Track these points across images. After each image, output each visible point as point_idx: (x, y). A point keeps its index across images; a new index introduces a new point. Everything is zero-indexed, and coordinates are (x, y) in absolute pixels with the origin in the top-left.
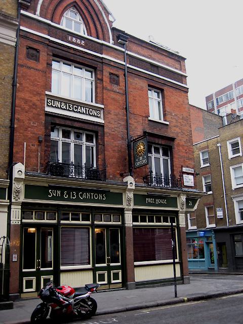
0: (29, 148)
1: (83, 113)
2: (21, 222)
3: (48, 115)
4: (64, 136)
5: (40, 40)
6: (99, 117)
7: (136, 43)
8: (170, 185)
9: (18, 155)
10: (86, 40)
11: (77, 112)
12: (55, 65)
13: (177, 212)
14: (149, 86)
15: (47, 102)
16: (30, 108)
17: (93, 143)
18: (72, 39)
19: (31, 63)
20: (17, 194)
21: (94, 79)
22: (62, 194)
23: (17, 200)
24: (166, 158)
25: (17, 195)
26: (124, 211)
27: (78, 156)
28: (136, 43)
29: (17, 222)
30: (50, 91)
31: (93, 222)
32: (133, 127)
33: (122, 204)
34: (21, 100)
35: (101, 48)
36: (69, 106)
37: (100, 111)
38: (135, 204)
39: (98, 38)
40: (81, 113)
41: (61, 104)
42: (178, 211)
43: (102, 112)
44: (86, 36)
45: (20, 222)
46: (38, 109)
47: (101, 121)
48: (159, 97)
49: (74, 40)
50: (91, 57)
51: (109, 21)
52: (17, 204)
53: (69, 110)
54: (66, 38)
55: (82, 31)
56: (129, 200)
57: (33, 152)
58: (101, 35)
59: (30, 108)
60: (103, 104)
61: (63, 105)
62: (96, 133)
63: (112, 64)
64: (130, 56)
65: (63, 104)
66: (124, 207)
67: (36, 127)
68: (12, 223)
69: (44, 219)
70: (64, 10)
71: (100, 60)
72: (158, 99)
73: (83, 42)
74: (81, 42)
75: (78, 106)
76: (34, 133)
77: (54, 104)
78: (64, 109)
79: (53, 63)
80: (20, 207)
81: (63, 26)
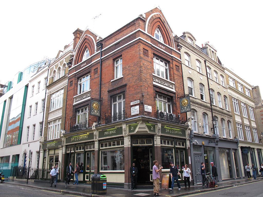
3: (155, 86)
6: (173, 89)
13: (123, 137)
14: (154, 54)
18: (160, 46)
19: (146, 58)
21: (168, 67)
23: (159, 134)
31: (174, 146)
33: (122, 134)
36: (161, 82)
42: (186, 139)
44: (163, 43)
47: (174, 90)
48: (166, 66)
53: (161, 84)
55: (161, 40)
58: (170, 45)
60: (174, 82)
64: (104, 51)
66: (186, 138)
71: (170, 57)
73: (164, 47)
80: (160, 137)
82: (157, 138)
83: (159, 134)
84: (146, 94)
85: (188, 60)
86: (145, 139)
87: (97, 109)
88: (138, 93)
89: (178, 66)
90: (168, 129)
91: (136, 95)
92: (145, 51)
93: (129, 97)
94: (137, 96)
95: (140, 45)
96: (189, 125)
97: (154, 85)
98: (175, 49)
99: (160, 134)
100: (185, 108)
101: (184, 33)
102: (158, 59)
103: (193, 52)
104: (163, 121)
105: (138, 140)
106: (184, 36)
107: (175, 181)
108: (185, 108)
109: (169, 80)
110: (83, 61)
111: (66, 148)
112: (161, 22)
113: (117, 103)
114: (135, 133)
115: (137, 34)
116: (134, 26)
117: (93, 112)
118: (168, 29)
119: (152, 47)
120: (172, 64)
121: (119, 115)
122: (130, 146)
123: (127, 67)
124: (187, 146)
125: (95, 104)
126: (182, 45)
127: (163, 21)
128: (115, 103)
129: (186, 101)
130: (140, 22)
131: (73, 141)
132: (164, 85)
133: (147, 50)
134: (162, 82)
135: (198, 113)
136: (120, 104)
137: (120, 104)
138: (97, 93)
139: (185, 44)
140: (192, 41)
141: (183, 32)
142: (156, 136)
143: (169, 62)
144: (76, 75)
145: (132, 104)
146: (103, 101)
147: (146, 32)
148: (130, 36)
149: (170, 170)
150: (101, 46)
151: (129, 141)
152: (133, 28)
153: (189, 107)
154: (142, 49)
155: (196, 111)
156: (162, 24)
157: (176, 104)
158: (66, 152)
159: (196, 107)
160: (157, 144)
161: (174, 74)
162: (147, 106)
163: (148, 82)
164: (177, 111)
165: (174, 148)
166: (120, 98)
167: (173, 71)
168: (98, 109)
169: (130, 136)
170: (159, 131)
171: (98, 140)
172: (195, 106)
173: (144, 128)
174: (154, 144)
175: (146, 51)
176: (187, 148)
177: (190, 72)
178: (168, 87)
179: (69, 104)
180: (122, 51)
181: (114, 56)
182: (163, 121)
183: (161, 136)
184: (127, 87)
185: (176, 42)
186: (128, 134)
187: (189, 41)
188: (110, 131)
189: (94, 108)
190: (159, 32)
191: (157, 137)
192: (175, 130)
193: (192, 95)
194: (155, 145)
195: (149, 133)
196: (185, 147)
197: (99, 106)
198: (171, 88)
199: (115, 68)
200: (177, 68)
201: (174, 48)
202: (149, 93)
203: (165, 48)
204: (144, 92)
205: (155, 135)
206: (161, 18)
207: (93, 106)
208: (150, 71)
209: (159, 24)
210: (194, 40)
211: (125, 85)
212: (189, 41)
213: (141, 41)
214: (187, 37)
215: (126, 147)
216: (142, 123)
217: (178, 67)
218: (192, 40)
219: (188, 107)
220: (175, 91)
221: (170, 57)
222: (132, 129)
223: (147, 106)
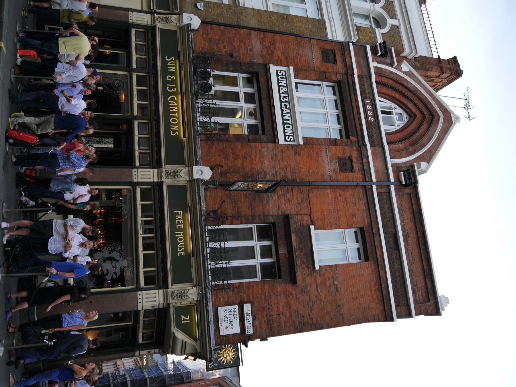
0: (221, 42)
5: (385, 292)
7: (417, 234)
8: (213, 283)
9: (209, 30)
16: (267, 47)
20: (178, 295)
22: (180, 229)
27: (235, 253)
28: (417, 234)
29: (132, 18)
32: (289, 196)
33: (167, 163)
34: (273, 39)
46: (268, 57)
51: (405, 73)
52: (153, 20)
54: (366, 97)
56: (182, 294)
57: (217, 46)
59: (267, 47)
61: (284, 89)
63: (365, 160)
64: (389, 193)
66: (170, 286)
67: (247, 52)
68: (130, 13)
69: (142, 200)
75: (289, 109)
76: (238, 48)
77: (281, 78)
80: (156, 180)
88: (271, 327)
91: (266, 319)
93: (263, 297)
94: (263, 322)
110: (377, 98)
111: (146, 27)
115: (379, 149)
116: (424, 295)
121: (211, 111)
123: (336, 282)
128: (241, 82)
131: (164, 64)
136: (250, 253)
137: (250, 253)
138: (289, 174)
144: (349, 76)
145: (247, 307)
152: (420, 294)
158: (134, 25)
166: (265, 252)
171: (162, 183)
174: (137, 168)
179: (273, 43)
180: (376, 260)
181: (371, 231)
184: (289, 287)
186: (171, 305)
188: (185, 234)
194: (135, 170)
211: (293, 281)
215: (134, 173)
222: (184, 320)
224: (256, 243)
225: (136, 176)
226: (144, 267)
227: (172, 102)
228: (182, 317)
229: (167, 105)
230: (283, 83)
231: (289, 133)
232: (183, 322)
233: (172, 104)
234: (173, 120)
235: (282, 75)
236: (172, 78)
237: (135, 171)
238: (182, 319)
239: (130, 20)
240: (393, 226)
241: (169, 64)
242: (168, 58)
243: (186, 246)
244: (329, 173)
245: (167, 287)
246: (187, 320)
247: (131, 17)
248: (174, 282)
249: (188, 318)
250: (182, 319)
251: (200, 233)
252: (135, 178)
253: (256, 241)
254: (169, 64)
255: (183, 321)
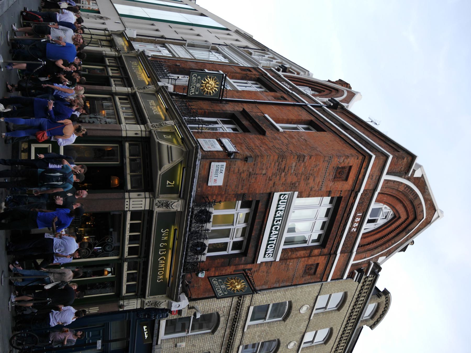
1: (269, 237)
2: (127, 211)
3: (270, 197)
4: (234, 243)
6: (264, 257)
10: (357, 233)
11: (271, 230)
12: (327, 200)
14: (339, 199)
15: (284, 195)
17: (232, 250)
18: (358, 217)
21: (311, 244)
23: (156, 204)
24: (230, 246)
25: (162, 204)
26: (141, 298)
30: (298, 197)
31: (126, 260)
35: (348, 251)
36: (279, 220)
37: (272, 256)
38: (160, 214)
39: (359, 247)
40: (270, 235)
41: (281, 210)
43: (271, 259)
44: (362, 231)
45: (128, 209)
47: (261, 259)
48: (314, 241)
49: (358, 219)
50: (339, 233)
53: (274, 220)
55: (367, 227)
58: (362, 249)
60: (281, 259)
62: (244, 254)
65: (281, 213)
66: (147, 297)
69: (130, 232)
70: (389, 204)
71: (334, 249)
72: (311, 241)
74: (355, 228)
77: (282, 202)
78: (275, 215)
79: (329, 198)
80: (147, 208)
81: (374, 205)
82: (145, 198)
83: (156, 204)
84: (251, 170)
85: (315, 341)
86: (142, 173)
87: (202, 90)
89: (315, 273)
90: (169, 236)
92: (314, 268)
95: (358, 159)
96: (179, 303)
97: (272, 195)
98: (352, 262)
99: (157, 210)
100: (223, 287)
101: (386, 292)
102: (327, 215)
103: (346, 319)
104: (188, 215)
105: (140, 156)
106: (378, 293)
107: (37, 322)
108: (223, 287)
109: (282, 247)
112: (407, 222)
113: (220, 125)
114: (157, 140)
117: (197, 77)
118: (393, 242)
119: (354, 191)
120: (320, 255)
122: (124, 134)
124: (126, 302)
125: (213, 84)
126: (362, 281)
127: (410, 228)
129: (238, 287)
130: (405, 160)
132: (273, 229)
133: (346, 179)
134: (280, 223)
135: (209, 337)
139: (344, 341)
140: (371, 316)
141: (389, 290)
142: (151, 196)
143: (323, 246)
146: (220, 104)
147: (385, 177)
148: (369, 144)
149: (61, 155)
150: (332, 104)
151: (136, 134)
153: (226, 293)
154: (348, 163)
155: (213, 332)
156: (404, 226)
157: (229, 265)
159: (223, 332)
160: (130, 199)
161: (298, 258)
162: (224, 169)
163: (278, 177)
164: (214, 269)
165: (122, 260)
167: (304, 257)
168: (202, 93)
169: (147, 136)
170: (162, 204)
172: (225, 325)
173: (170, 159)
174: (129, 192)
175: (344, 176)
176: (121, 302)
177: (291, 346)
178: (268, 241)
182: (188, 215)
183: (150, 212)
185: (366, 265)
187: (370, 308)
189: (205, 81)
190: (385, 221)
191: (148, 200)
192: (166, 261)
193: (251, 320)
194: (127, 195)
195: (159, 173)
196: (123, 295)
197: (210, 93)
198: (266, 251)
199: (295, 126)
200: (311, 269)
201: (354, 260)
202: (253, 180)
203: (353, 232)
204: (254, 164)
205: (152, 195)
206: (416, 222)
207: (210, 78)
208: (303, 184)
209: (403, 216)
210: (372, 322)
212: (370, 308)
213: (366, 160)
214: (380, 300)
216: (183, 151)
217: (313, 271)
218: (372, 318)
219: (225, 291)
220: (259, 262)
221: (334, 249)
222: (169, 184)
223: (224, 172)
224: (230, 240)
225: (128, 206)
226: (131, 220)
227: (161, 261)
228: (168, 182)
229: (156, 264)
230: (282, 207)
231: (282, 207)
232: (167, 186)
233: (161, 263)
234: (160, 273)
235: (284, 199)
236: (164, 244)
237: (127, 202)
238: (167, 184)
239: (125, 208)
240: (369, 199)
241: (163, 235)
242: (163, 231)
243: (164, 275)
244: (322, 182)
245: (144, 297)
246: (172, 185)
247: (127, 205)
248: (152, 294)
249: (173, 183)
250: (167, 184)
251: (178, 274)
252: (127, 208)
253: (231, 239)
254: (163, 235)
255: (168, 185)
